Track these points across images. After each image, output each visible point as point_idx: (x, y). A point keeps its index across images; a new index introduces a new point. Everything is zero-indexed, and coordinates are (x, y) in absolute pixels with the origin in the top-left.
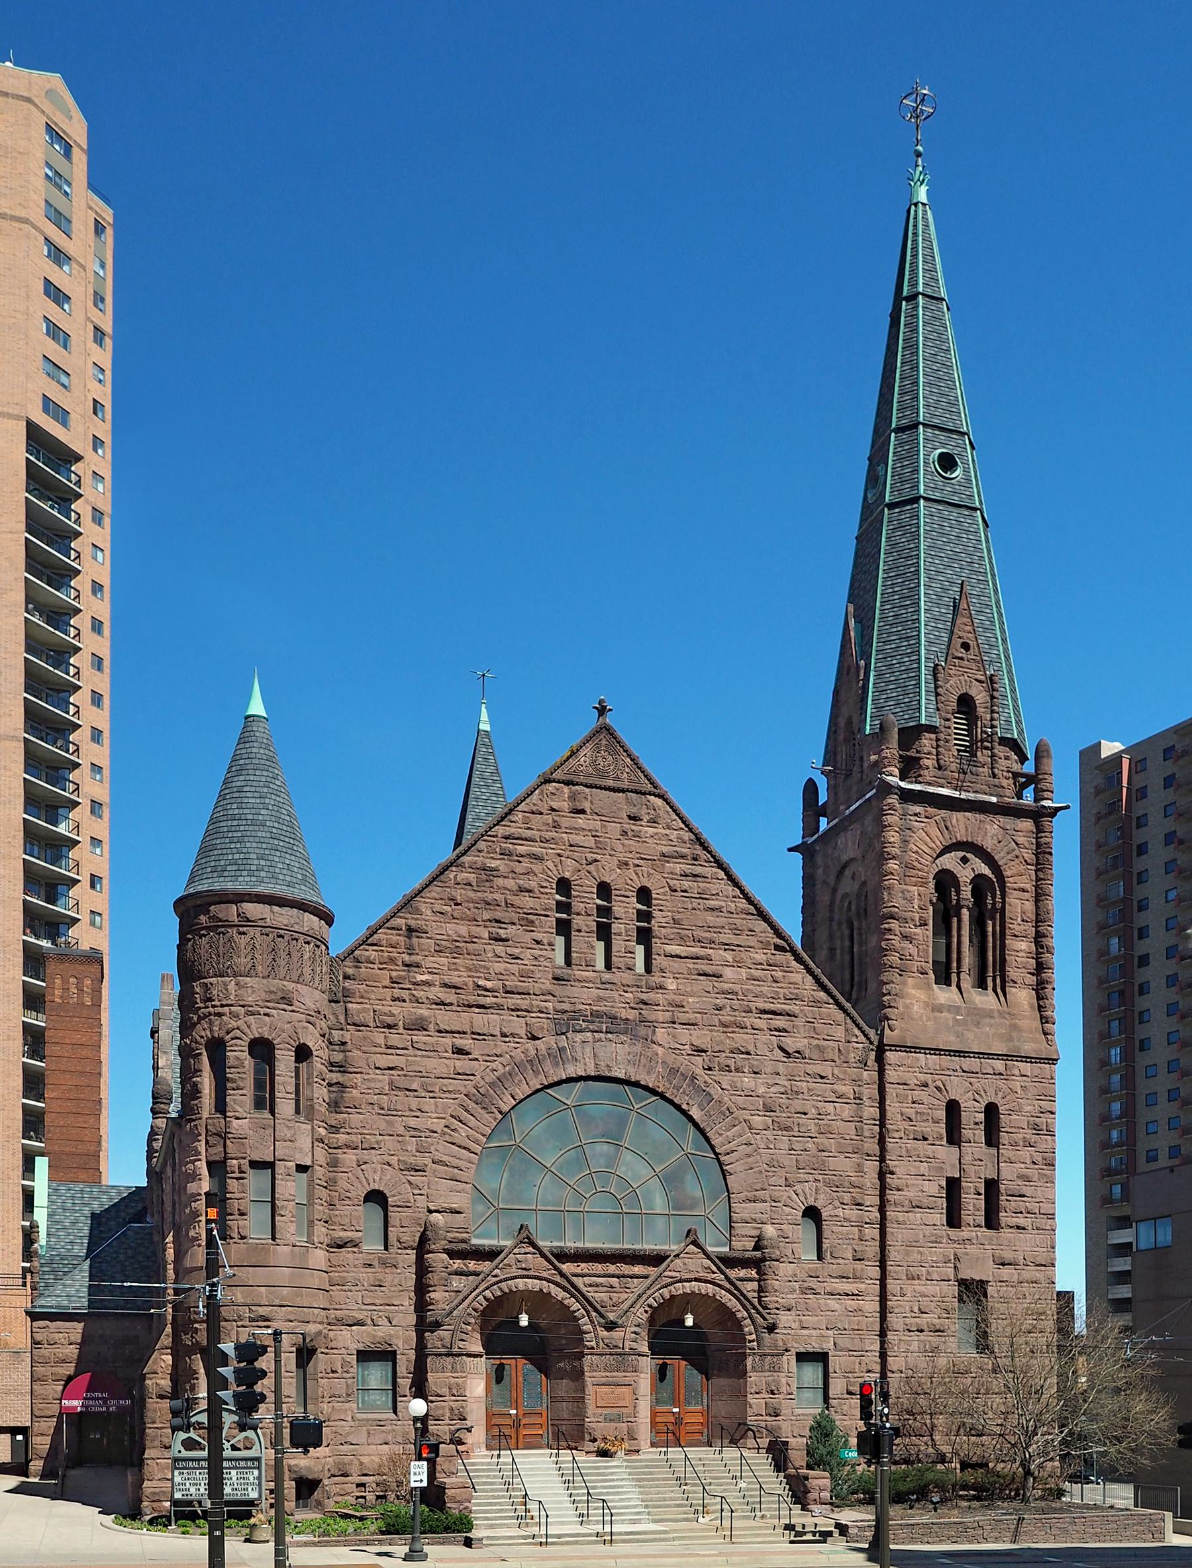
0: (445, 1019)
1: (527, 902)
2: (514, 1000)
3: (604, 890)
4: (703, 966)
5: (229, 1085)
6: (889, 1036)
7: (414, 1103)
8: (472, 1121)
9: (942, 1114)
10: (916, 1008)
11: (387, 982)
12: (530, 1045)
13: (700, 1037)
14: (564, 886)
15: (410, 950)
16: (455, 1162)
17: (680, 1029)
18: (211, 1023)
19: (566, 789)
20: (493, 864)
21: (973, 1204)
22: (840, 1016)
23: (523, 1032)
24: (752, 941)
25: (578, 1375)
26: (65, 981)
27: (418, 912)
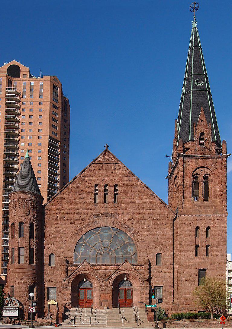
1: (88, 190)
4: (131, 200)
15: (61, 202)
21: (202, 250)
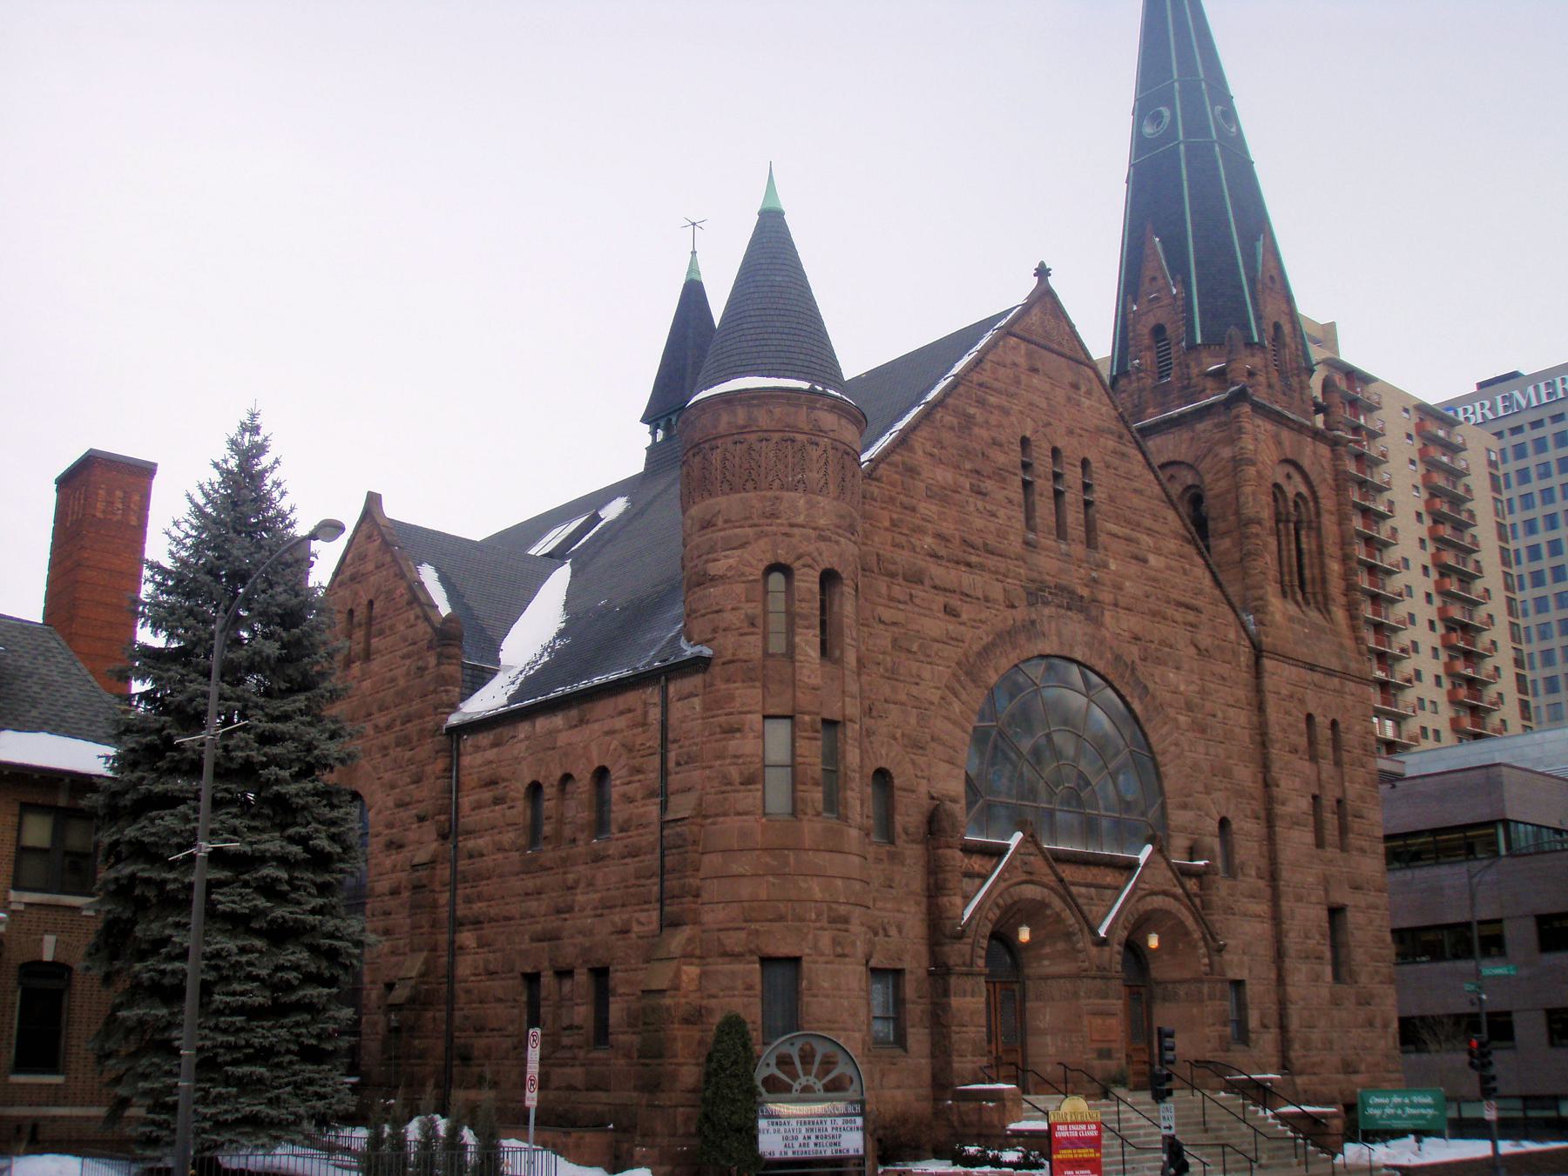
2: (992, 562)
3: (1056, 452)
9: (1303, 726)
10: (1278, 617)
11: (887, 524)
14: (1025, 442)
19: (1023, 346)
20: (972, 411)
23: (1001, 597)
27: (911, 449)
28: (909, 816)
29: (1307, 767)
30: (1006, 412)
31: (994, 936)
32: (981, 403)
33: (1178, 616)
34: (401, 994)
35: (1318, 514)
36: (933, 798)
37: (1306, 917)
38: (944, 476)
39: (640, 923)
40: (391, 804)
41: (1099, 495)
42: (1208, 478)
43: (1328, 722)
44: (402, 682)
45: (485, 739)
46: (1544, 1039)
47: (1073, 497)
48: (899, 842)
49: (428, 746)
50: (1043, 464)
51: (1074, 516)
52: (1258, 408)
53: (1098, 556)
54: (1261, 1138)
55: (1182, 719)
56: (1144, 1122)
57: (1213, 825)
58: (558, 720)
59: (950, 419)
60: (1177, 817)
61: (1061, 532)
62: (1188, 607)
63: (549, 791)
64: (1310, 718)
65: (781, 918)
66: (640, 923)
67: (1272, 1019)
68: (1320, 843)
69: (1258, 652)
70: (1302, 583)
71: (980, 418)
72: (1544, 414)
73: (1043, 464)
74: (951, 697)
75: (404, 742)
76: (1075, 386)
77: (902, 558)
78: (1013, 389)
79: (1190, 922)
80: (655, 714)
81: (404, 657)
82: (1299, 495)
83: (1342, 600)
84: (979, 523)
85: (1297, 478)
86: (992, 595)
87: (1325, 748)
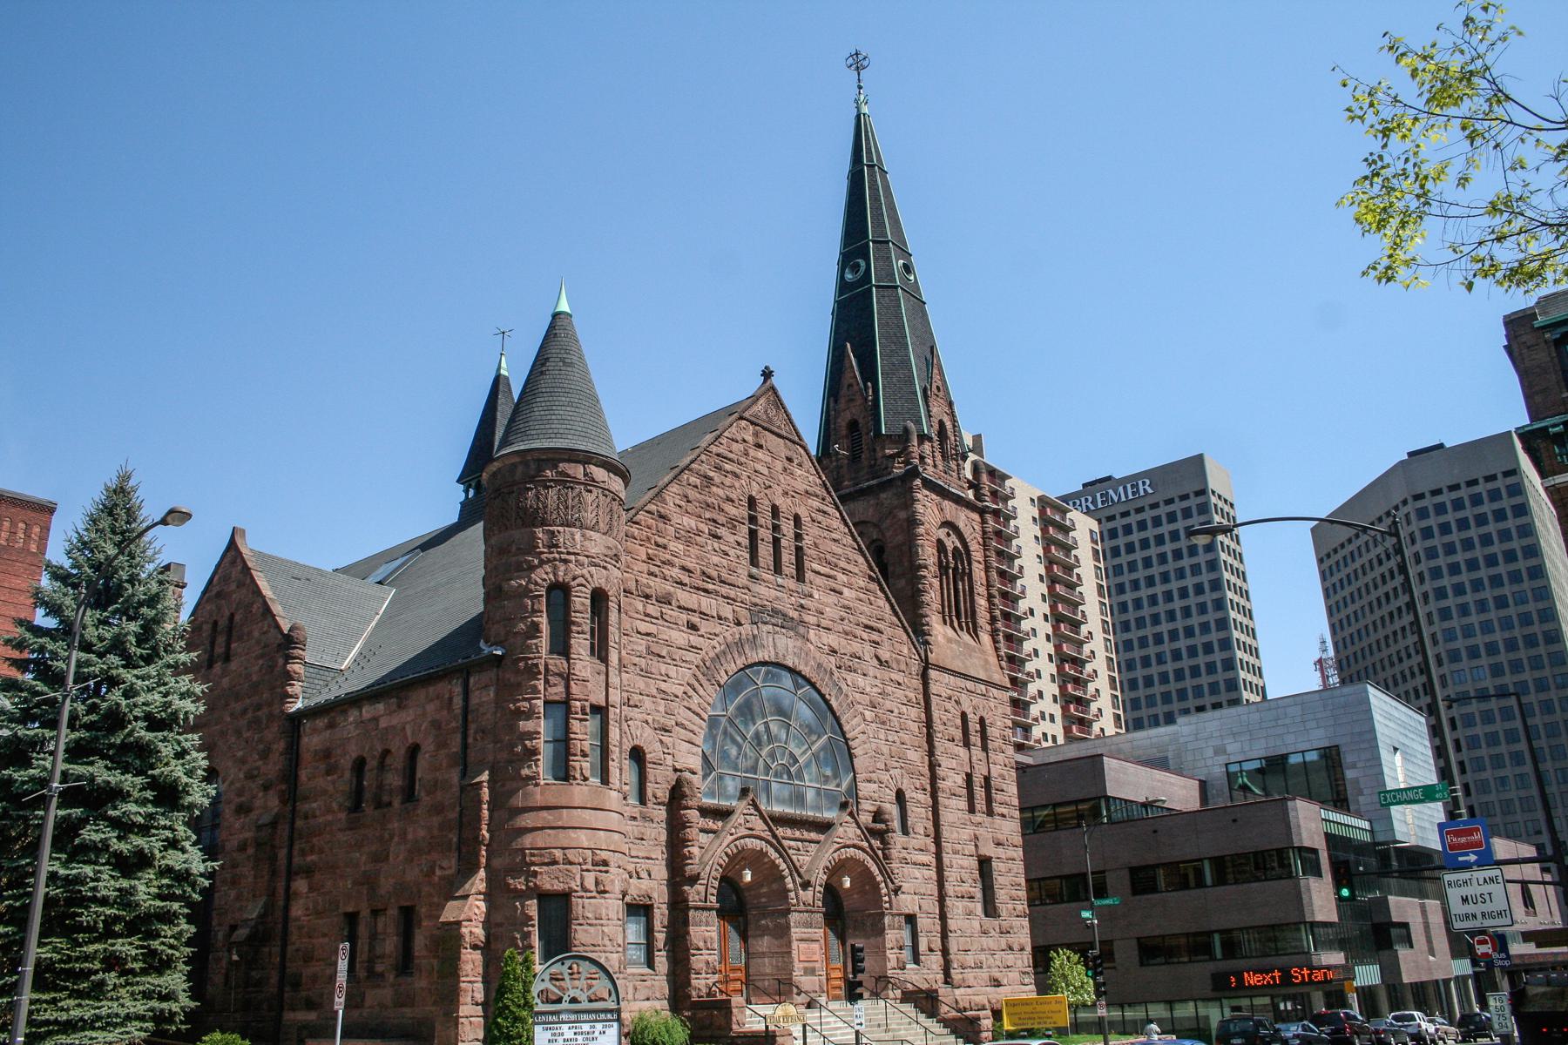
0: (684, 597)
1: (732, 510)
2: (724, 590)
3: (775, 511)
5: (574, 628)
6: (932, 657)
7: (663, 668)
8: (701, 692)
9: (959, 722)
10: (940, 638)
11: (644, 557)
12: (736, 629)
13: (832, 640)
16: (692, 727)
17: (822, 632)
18: (555, 568)
20: (711, 474)
22: (905, 637)
23: (731, 617)
24: (856, 570)
25: (783, 932)
26: (13, 524)
27: (664, 501)
28: (659, 787)
29: (962, 752)
30: (737, 476)
31: (724, 879)
32: (718, 468)
33: (865, 636)
34: (242, 933)
35: (970, 564)
36: (676, 770)
37: (961, 868)
38: (691, 522)
39: (442, 868)
40: (241, 776)
41: (807, 541)
42: (888, 534)
43: (977, 718)
44: (255, 678)
45: (321, 723)
46: (1136, 960)
47: (787, 543)
48: (650, 805)
49: (275, 728)
50: (765, 519)
51: (788, 557)
52: (929, 485)
53: (806, 588)
54: (930, 1036)
55: (867, 713)
56: (841, 1024)
57: (892, 795)
58: (380, 707)
59: (694, 480)
60: (865, 789)
61: (778, 569)
62: (871, 628)
63: (372, 763)
64: (964, 715)
65: (554, 862)
66: (442, 868)
67: (937, 944)
68: (972, 810)
69: (926, 666)
70: (961, 615)
71: (717, 480)
72: (1131, 507)
73: (765, 519)
74: (691, 692)
75: (255, 724)
76: (790, 460)
77: (657, 586)
78: (743, 460)
79: (874, 869)
80: (458, 702)
81: (257, 658)
82: (955, 548)
83: (988, 628)
84: (716, 559)
85: (953, 537)
86: (723, 615)
87: (975, 739)
